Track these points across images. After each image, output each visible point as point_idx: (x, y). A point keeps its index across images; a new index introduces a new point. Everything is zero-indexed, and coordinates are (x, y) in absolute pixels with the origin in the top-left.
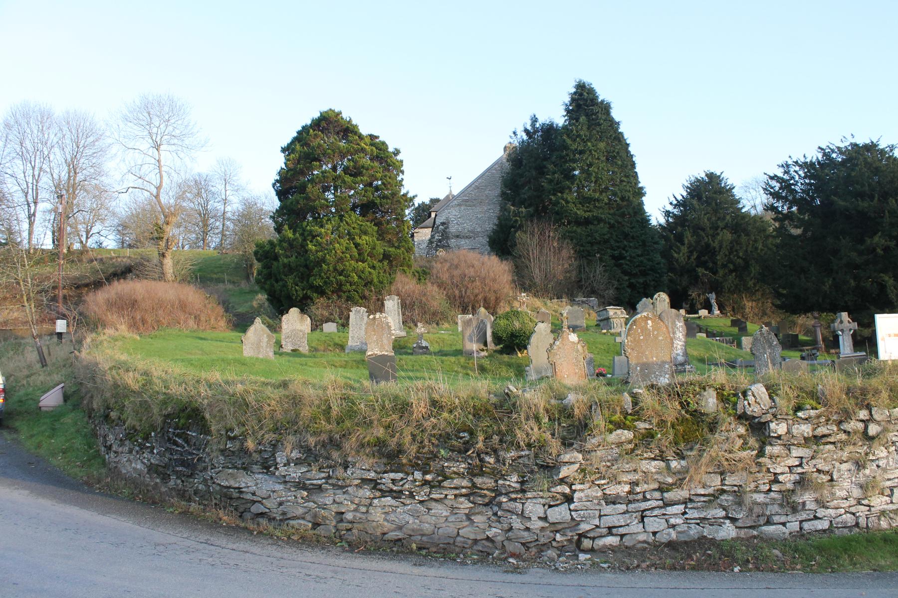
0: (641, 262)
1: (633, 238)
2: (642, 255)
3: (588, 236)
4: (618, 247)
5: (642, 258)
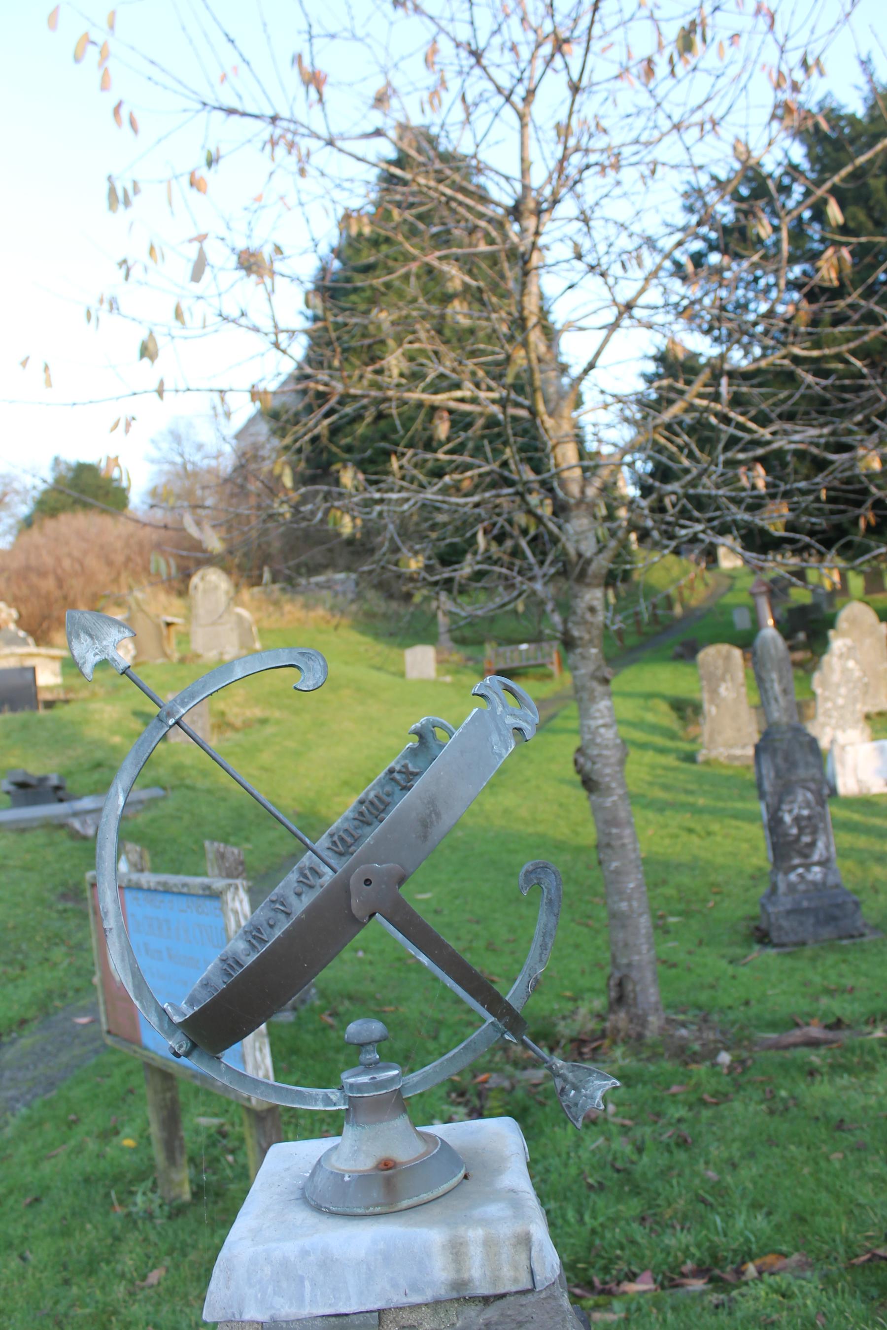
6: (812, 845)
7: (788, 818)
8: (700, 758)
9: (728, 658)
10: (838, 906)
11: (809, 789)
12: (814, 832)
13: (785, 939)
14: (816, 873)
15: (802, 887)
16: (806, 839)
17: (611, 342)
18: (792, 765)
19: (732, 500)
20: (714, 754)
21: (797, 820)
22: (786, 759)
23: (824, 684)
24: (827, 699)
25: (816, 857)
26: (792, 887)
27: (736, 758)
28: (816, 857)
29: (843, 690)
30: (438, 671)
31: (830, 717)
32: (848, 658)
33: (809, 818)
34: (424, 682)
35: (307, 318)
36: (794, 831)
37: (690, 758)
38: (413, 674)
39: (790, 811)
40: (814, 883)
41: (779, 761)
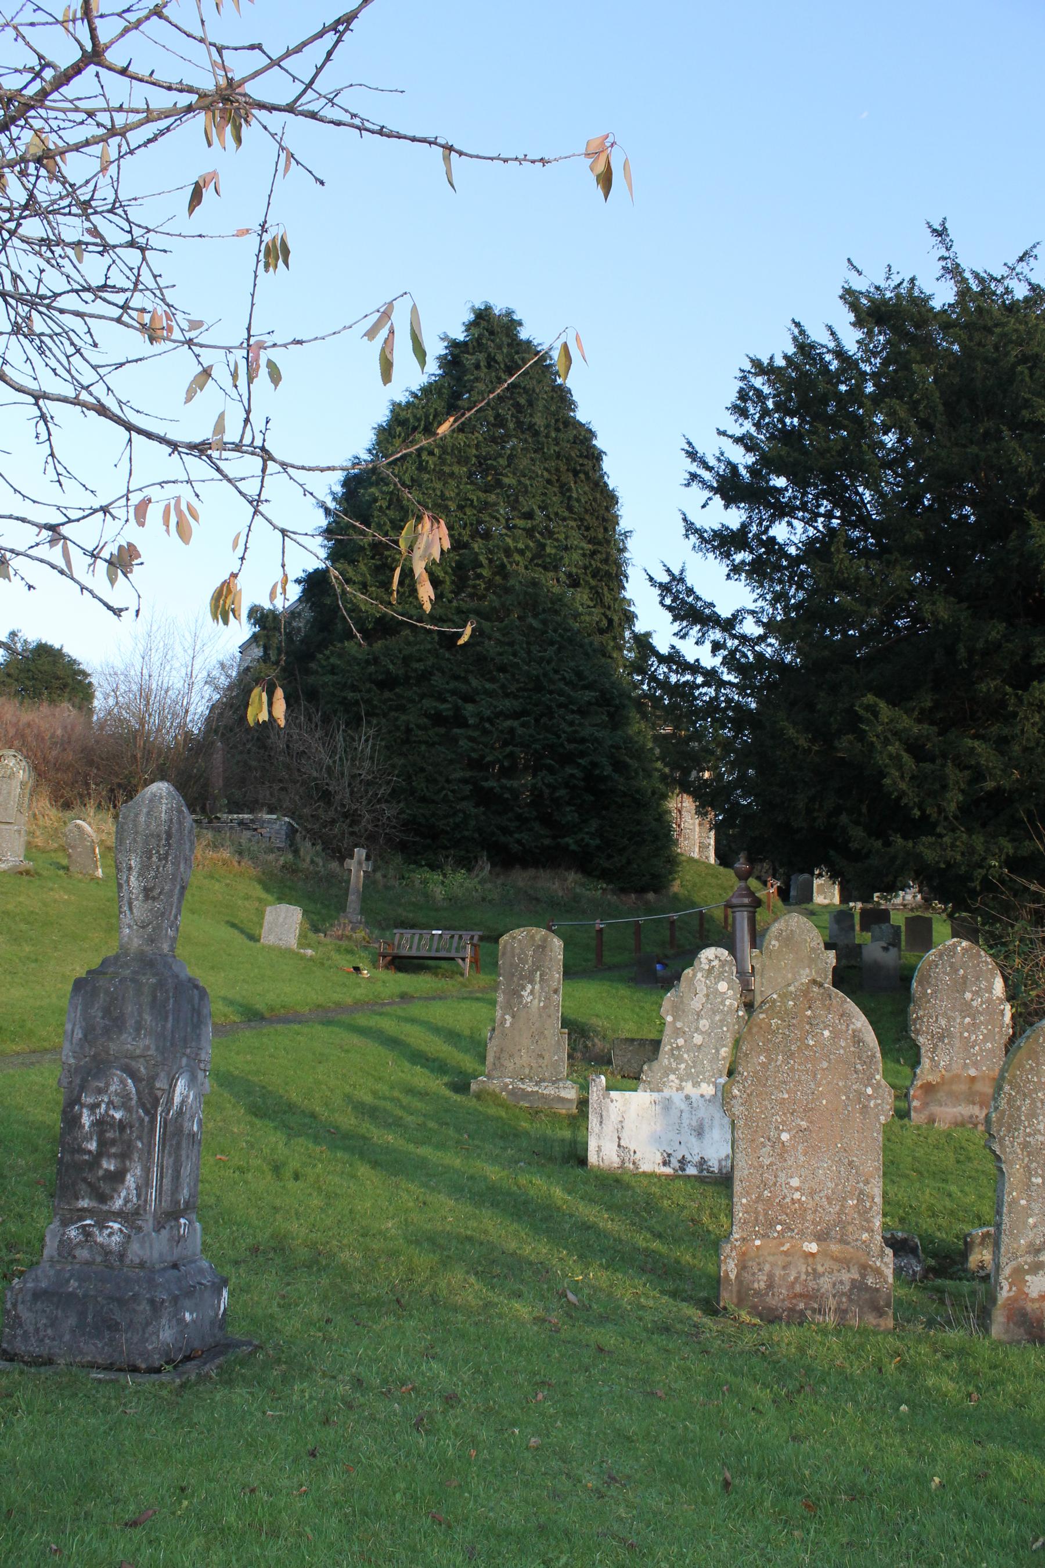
0: (512, 731)
1: (502, 669)
2: (516, 715)
3: (376, 661)
4: (454, 692)
5: (516, 724)
6: (117, 1177)
7: (86, 1120)
8: (474, 1087)
9: (542, 948)
10: (121, 1302)
11: (133, 1074)
12: (124, 1156)
13: (20, 1347)
14: (112, 1236)
15: (83, 1254)
16: (109, 1165)
17: (680, 566)
18: (116, 1023)
19: (560, 706)
20: (495, 1085)
21: (101, 1125)
22: (107, 1012)
23: (678, 1010)
24: (678, 1032)
25: (118, 1204)
26: (66, 1248)
27: (526, 1095)
28: (118, 1204)
29: (704, 1024)
30: (303, 936)
31: (679, 1059)
32: (719, 978)
33: (122, 1126)
34: (286, 953)
35: (332, 493)
36: (93, 1146)
37: (461, 1087)
38: (268, 938)
39: (93, 1107)
40: (106, 1251)
41: (96, 1012)
